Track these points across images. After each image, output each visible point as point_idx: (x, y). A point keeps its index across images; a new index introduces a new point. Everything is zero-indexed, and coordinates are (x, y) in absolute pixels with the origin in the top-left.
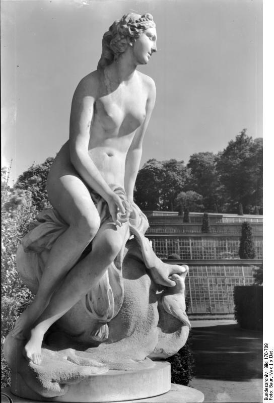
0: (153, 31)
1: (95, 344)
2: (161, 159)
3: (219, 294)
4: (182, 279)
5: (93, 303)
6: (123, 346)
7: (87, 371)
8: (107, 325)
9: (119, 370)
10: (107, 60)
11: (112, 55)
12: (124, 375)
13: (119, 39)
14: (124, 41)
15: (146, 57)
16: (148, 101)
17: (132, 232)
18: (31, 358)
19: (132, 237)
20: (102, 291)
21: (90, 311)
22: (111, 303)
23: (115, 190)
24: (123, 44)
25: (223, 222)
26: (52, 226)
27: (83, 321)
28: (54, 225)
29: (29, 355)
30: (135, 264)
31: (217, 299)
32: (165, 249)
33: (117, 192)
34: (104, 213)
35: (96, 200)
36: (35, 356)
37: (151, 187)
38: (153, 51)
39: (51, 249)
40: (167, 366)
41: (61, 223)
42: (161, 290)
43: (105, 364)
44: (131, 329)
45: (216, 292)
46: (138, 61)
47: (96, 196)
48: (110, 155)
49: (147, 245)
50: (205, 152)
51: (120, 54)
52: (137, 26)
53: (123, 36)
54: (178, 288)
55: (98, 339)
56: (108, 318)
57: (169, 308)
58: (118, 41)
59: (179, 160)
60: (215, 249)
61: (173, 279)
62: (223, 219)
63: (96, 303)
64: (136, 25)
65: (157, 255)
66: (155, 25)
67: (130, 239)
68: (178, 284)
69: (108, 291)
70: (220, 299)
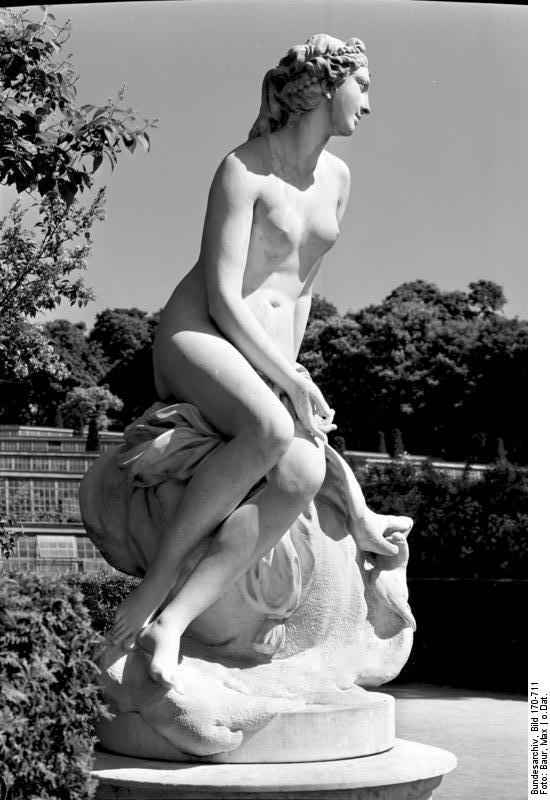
1: (266, 659)
4: (403, 537)
5: (261, 583)
9: (324, 704)
10: (272, 121)
13: (308, 83)
14: (317, 89)
15: (351, 121)
16: (339, 203)
21: (254, 597)
24: (312, 92)
26: (187, 435)
32: (54, 503)
38: (365, 111)
41: (207, 430)
42: (374, 559)
44: (325, 626)
46: (336, 126)
48: (274, 305)
50: (129, 307)
51: (306, 111)
52: (341, 62)
53: (315, 80)
54: (399, 558)
55: (267, 650)
56: (288, 611)
57: (385, 595)
58: (306, 87)
61: (395, 541)
63: (267, 584)
64: (340, 59)
65: (368, 503)
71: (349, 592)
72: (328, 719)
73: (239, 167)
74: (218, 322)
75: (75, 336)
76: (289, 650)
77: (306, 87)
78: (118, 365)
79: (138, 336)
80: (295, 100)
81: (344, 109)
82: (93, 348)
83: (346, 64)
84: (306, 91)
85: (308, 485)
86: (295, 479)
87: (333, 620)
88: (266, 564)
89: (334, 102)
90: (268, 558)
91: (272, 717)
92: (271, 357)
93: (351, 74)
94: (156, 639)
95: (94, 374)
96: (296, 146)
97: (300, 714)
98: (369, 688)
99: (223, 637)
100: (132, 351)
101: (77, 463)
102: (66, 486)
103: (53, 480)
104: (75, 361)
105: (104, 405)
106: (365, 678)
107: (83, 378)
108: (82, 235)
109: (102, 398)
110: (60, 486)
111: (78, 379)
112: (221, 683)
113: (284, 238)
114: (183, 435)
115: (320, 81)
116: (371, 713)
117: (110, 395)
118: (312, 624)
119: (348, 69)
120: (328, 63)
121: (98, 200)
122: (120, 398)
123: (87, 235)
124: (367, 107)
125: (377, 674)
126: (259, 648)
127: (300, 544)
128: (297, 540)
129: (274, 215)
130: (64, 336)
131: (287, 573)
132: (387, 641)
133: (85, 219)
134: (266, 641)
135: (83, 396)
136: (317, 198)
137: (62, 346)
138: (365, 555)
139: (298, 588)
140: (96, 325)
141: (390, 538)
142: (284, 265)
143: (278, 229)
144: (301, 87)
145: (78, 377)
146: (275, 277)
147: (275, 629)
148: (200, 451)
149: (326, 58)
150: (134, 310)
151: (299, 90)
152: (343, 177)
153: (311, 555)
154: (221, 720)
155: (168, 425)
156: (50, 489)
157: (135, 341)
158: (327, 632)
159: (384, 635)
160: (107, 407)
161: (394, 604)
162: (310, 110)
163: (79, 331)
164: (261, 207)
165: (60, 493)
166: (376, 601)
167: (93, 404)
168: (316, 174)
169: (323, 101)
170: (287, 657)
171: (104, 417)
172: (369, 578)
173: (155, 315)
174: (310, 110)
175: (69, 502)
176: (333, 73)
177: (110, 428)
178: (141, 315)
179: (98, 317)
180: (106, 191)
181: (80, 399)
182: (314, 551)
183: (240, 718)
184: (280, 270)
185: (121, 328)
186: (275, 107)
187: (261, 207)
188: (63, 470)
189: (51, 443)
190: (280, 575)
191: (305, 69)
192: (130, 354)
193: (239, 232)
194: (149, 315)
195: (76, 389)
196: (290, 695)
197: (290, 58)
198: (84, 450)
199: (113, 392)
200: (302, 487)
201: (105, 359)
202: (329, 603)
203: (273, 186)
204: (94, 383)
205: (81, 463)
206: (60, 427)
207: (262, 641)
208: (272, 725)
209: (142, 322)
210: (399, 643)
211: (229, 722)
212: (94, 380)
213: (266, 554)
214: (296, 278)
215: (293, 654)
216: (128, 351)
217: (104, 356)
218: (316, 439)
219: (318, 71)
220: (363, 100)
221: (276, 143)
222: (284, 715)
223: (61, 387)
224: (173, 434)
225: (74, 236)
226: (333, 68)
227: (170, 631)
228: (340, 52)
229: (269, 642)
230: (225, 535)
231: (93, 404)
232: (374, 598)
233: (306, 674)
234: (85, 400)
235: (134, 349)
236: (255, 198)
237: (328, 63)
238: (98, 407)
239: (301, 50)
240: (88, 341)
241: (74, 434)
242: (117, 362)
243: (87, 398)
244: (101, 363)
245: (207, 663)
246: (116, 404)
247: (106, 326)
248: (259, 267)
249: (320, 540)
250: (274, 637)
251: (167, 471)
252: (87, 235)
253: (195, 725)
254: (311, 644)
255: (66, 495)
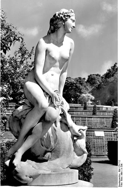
0: (73, 18)
2: (75, 76)
3: (100, 145)
5: (44, 142)
6: (57, 161)
7: (41, 172)
8: (50, 153)
9: (55, 172)
10: (51, 30)
11: (55, 28)
12: (58, 174)
13: (58, 21)
14: (61, 22)
15: (70, 30)
16: (70, 50)
17: (62, 110)
18: (17, 166)
19: (62, 113)
20: (49, 137)
21: (43, 146)
22: (52, 142)
23: (54, 92)
25: (103, 110)
27: (39, 151)
28: (27, 106)
29: (15, 165)
30: (66, 126)
31: (99, 148)
33: (56, 92)
34: (50, 101)
35: (46, 95)
36: (18, 165)
37: (71, 91)
38: (74, 27)
39: (25, 117)
40: (77, 171)
41: (30, 106)
42: (76, 137)
43: (49, 169)
44: (61, 152)
45: (99, 145)
46: (66, 31)
47: (47, 94)
48: (52, 75)
49: (69, 117)
52: (66, 15)
53: (60, 20)
55: (46, 159)
56: (51, 149)
57: (78, 146)
58: (58, 22)
59: (82, 77)
60: (99, 123)
62: (103, 108)
64: (66, 15)
66: (75, 15)
67: (61, 113)
68: (82, 134)
69: (51, 137)
70: (101, 148)
71: (68, 145)
72: (54, 176)
73: (42, 41)
74: (36, 80)
75: (83, 81)
76: (52, 159)
77: (58, 22)
78: (94, 88)
79: (99, 81)
80: (56, 26)
81: (68, 27)
82: (87, 84)
83: (67, 16)
84: (58, 23)
85: (52, 119)
86: (49, 117)
87: (63, 152)
88: (45, 138)
89: (65, 25)
90: (45, 136)
91: (40, 175)
92: (47, 88)
93: (69, 18)
94: (15, 156)
95: (88, 91)
96: (57, 36)
97: (47, 174)
98: (71, 168)
99: (37, 155)
100: (97, 85)
101: (81, 113)
102: (77, 119)
103: (86, 117)
104: (83, 88)
105: (89, 98)
106: (72, 166)
107: (85, 92)
108: (29, 58)
109: (89, 96)
110: (76, 118)
111: (83, 92)
112: (32, 166)
113: (53, 59)
114: (24, 107)
115: (61, 20)
116: (67, 175)
117: (91, 96)
118: (58, 152)
119: (68, 17)
120: (63, 16)
121: (32, 50)
122: (94, 96)
123: (30, 58)
124: (75, 26)
125: (75, 165)
126: (44, 158)
127: (54, 133)
128: (53, 132)
129: (50, 53)
130: (80, 81)
131: (50, 140)
132: (80, 157)
133: (30, 54)
134: (45, 157)
135: (84, 96)
136: (65, 48)
137: (80, 84)
138: (73, 136)
139: (52, 143)
140: (88, 78)
141: (79, 131)
142: (54, 65)
143: (51, 57)
144: (57, 22)
145: (83, 91)
146: (52, 68)
147: (47, 153)
148: (28, 110)
149: (62, 15)
150: (98, 74)
151: (56, 23)
152: (72, 43)
153: (56, 135)
154: (27, 175)
155: (21, 104)
156: (79, 119)
157: (98, 82)
158: (62, 155)
159: (79, 155)
160: (90, 99)
161: (81, 148)
162: (60, 27)
163: (84, 80)
164: (47, 51)
165: (75, 120)
166: (76, 147)
167: (87, 98)
168: (63, 43)
169: (62, 25)
170: (52, 160)
171: (90, 101)
172: (74, 141)
173: (103, 75)
174: (60, 27)
175: (78, 122)
176: (64, 18)
177: (91, 104)
178: (99, 76)
179: (89, 76)
180: (34, 48)
181: (84, 97)
182: (57, 135)
183: (32, 175)
184: (54, 67)
185: (94, 79)
186: (52, 27)
187: (47, 51)
188: (78, 115)
189: (75, 108)
190: (48, 140)
191: (57, 17)
192: (97, 85)
193: (42, 58)
194: (101, 76)
195: (83, 94)
196: (48, 170)
197: (55, 16)
198: (83, 110)
199: (92, 95)
200: (51, 119)
201: (90, 87)
202: (62, 147)
203: (51, 47)
204: (87, 93)
205: (78, 113)
206: (78, 104)
207: (44, 157)
208: (40, 176)
209: (100, 77)
210: (82, 157)
211: (29, 176)
212: (87, 92)
213: (45, 134)
214: (58, 68)
215: (53, 160)
216: (96, 85)
217: (90, 86)
218: (56, 107)
219: (60, 18)
220: (73, 24)
221: (53, 36)
222: (43, 174)
223: (79, 94)
224: (23, 106)
225: (28, 59)
226: (64, 17)
227: (19, 154)
228: (66, 13)
229: (46, 157)
230: (33, 131)
231: (87, 98)
232: (76, 146)
233: (54, 165)
234: (85, 97)
235: (97, 84)
236: (46, 49)
237: (63, 16)
238: (88, 99)
239: (57, 13)
240: (86, 82)
241: (81, 105)
242: (93, 87)
243: (85, 96)
244: (89, 88)
245: (31, 161)
246: (93, 98)
247: (90, 79)
248: (48, 65)
249: (60, 132)
250: (47, 155)
251: (22, 116)
252: (30, 58)
253: (21, 176)
254: (58, 157)
255: (77, 121)
